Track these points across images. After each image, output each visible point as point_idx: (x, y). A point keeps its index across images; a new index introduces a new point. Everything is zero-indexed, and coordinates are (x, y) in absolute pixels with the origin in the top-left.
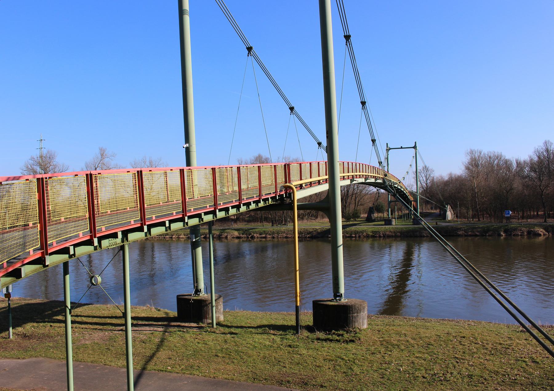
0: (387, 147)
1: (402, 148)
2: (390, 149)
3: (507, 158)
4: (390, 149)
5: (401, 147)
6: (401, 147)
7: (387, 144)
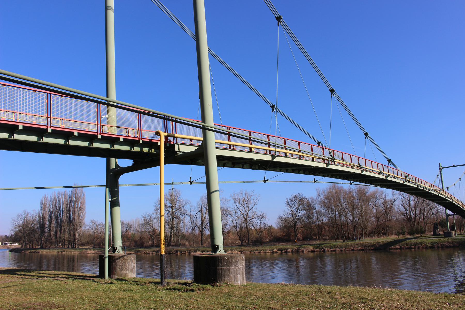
0: (440, 167)
1: (454, 166)
2: (443, 168)
3: (304, 196)
4: (443, 168)
5: (453, 165)
6: (453, 165)
7: (439, 164)
